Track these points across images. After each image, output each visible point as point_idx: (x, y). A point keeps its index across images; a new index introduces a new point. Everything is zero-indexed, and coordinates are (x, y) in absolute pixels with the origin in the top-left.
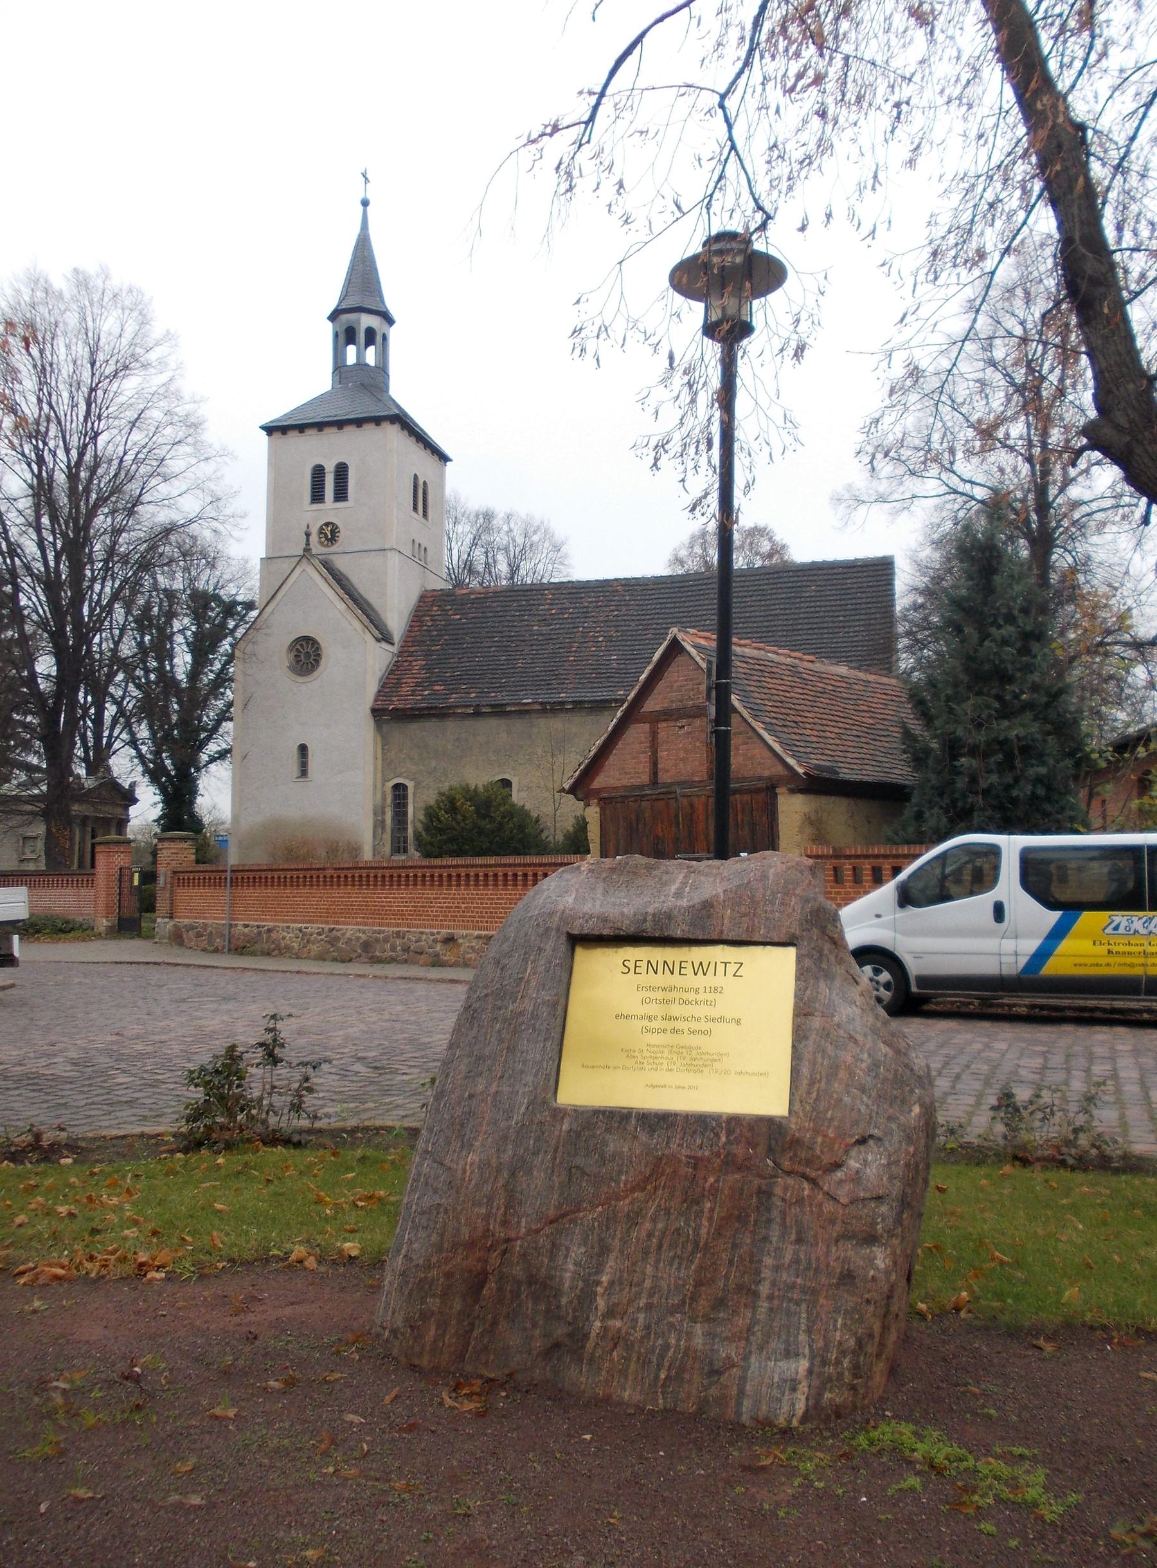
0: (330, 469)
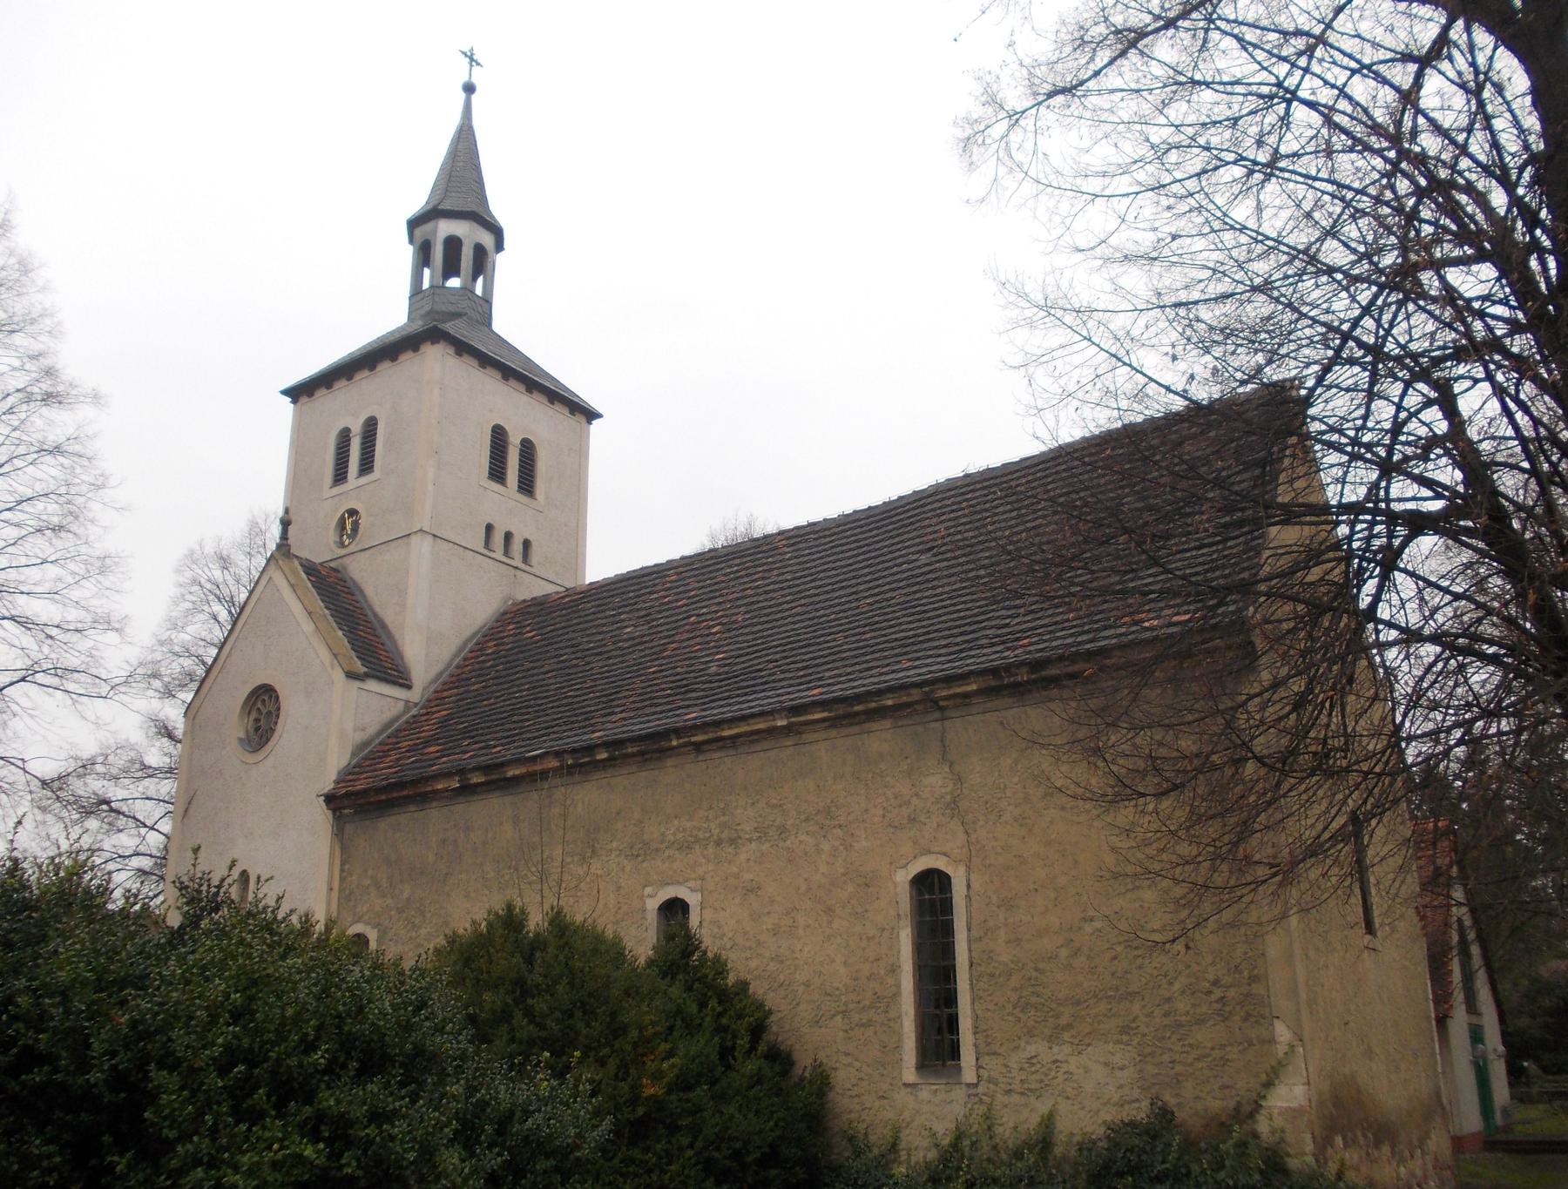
0: (356, 427)
